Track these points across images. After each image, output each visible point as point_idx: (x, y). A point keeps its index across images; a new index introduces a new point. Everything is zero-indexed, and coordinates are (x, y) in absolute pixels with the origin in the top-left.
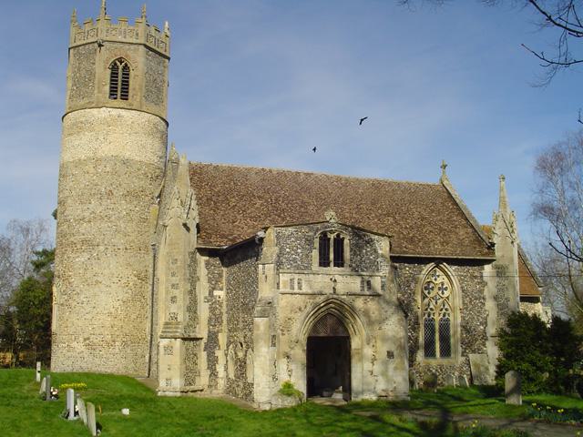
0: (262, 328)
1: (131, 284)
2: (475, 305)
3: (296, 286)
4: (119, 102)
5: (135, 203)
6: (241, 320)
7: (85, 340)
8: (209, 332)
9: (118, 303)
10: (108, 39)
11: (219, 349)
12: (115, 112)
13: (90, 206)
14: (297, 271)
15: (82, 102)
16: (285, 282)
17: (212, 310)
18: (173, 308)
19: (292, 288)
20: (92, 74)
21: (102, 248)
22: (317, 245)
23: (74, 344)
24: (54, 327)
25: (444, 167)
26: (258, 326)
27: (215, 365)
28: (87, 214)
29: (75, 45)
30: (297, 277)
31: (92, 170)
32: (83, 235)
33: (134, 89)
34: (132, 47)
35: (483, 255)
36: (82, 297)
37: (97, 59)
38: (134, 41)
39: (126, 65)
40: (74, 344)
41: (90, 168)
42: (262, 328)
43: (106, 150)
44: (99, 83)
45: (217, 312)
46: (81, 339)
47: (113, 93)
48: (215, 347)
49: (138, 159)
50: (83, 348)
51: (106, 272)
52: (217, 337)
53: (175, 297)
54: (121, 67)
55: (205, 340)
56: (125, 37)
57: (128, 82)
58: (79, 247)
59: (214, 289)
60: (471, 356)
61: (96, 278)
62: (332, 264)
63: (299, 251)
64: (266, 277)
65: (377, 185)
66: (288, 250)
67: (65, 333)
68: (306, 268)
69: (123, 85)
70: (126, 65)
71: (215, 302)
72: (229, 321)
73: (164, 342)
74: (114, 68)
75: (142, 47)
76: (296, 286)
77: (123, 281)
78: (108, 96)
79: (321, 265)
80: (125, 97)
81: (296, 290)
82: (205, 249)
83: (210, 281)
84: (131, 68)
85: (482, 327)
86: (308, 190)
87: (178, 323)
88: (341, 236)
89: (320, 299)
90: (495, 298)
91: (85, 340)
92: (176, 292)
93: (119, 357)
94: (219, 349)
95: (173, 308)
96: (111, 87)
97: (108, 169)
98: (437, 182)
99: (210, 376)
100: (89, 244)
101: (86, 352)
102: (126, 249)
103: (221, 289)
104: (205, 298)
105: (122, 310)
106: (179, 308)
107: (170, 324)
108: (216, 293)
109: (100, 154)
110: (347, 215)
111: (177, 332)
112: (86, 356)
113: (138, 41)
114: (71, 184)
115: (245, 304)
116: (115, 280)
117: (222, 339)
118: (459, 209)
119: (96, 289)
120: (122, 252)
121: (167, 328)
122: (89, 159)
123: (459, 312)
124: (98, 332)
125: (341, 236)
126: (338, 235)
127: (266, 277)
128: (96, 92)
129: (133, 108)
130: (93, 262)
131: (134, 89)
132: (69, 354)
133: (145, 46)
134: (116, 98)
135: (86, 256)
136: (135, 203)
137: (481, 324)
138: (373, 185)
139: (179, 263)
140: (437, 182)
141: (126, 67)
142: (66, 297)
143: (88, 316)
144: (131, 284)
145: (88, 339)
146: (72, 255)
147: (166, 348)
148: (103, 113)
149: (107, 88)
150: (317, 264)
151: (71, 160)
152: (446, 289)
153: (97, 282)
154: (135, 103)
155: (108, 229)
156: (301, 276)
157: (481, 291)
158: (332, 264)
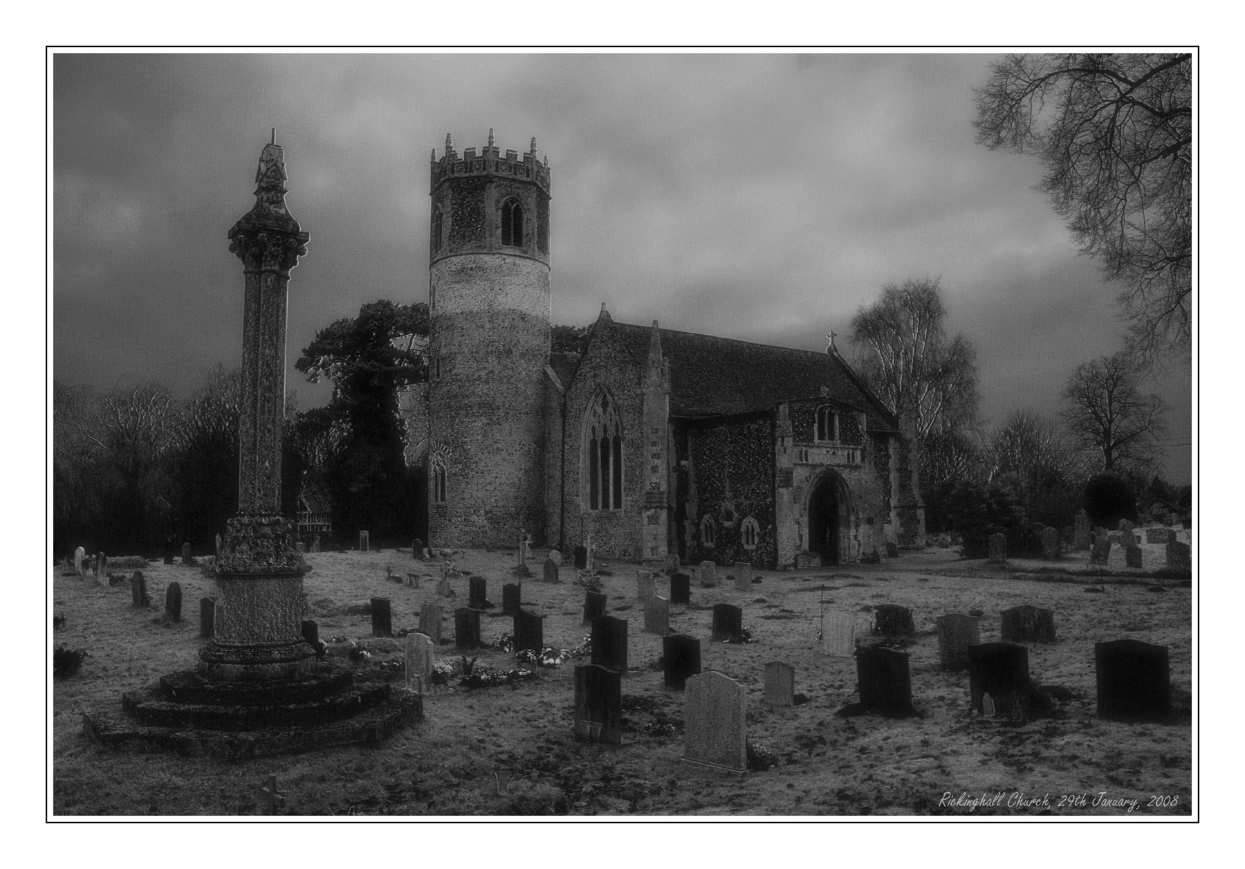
6: (727, 488)
47: (506, 241)
74: (506, 209)
87: (662, 493)
90: (899, 470)
91: (487, 513)
92: (657, 462)
100: (488, 407)
103: (687, 459)
108: (683, 463)
139: (660, 433)
141: (517, 208)
143: (489, 487)
151: (458, 311)
153: (498, 449)
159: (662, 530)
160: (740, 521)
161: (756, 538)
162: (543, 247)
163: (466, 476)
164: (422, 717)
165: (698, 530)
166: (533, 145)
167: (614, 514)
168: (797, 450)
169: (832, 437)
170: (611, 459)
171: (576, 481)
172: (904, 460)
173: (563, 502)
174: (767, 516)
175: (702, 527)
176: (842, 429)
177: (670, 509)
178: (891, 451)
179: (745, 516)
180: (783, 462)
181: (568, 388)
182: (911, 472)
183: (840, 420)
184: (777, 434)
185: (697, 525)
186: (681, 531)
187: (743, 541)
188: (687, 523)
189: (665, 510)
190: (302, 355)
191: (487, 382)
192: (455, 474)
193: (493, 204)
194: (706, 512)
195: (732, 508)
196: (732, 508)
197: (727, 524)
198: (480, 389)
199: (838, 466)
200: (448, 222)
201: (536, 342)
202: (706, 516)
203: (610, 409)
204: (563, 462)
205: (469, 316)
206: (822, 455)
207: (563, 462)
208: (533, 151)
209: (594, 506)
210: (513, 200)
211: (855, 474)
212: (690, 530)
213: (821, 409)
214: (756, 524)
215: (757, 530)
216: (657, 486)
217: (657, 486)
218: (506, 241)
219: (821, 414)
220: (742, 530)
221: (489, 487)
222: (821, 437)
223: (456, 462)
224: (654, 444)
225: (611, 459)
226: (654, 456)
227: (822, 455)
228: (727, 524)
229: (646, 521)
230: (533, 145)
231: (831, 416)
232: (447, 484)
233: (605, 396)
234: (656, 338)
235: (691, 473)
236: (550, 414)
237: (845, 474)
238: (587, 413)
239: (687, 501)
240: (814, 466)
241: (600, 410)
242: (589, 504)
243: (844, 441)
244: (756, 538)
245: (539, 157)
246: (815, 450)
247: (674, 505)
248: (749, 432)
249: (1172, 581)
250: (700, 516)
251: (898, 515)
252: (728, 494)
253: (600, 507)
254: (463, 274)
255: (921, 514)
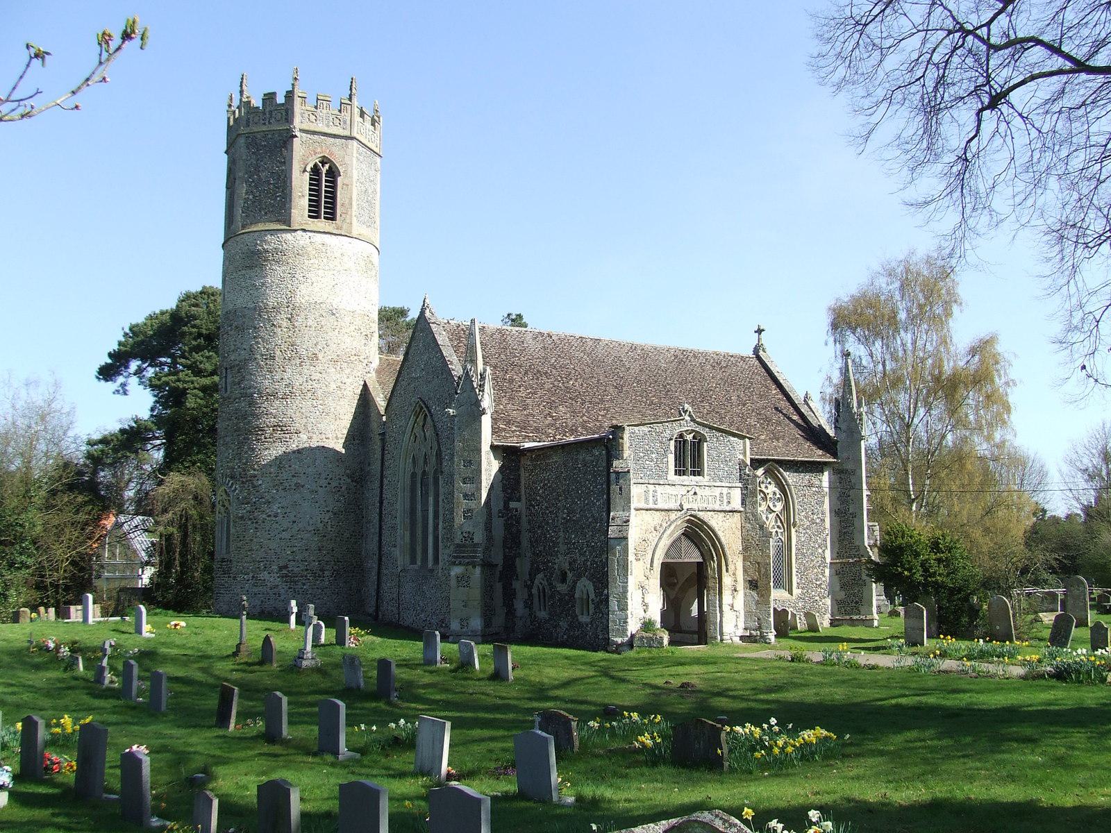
3: (651, 501)
4: (321, 224)
7: (281, 568)
8: (505, 556)
17: (508, 527)
19: (647, 500)
23: (264, 575)
25: (759, 331)
33: (343, 205)
40: (264, 575)
45: (514, 530)
46: (275, 568)
55: (500, 568)
61: (295, 480)
63: (654, 456)
64: (621, 489)
65: (682, 358)
67: (248, 559)
73: (456, 571)
78: (307, 213)
79: (678, 473)
80: (331, 216)
81: (651, 506)
91: (281, 568)
94: (517, 579)
103: (519, 500)
108: (513, 505)
111: (475, 557)
115: (109, 565)
116: (323, 482)
127: (621, 489)
132: (255, 590)
142: (248, 507)
143: (284, 535)
145: (286, 567)
147: (459, 579)
153: (298, 486)
160: (575, 583)
161: (591, 606)
164: (954, 375)
165: (531, 595)
170: (431, 499)
171: (394, 528)
175: (534, 591)
177: (487, 566)
179: (579, 576)
185: (530, 588)
186: (509, 595)
188: (517, 585)
190: (112, 351)
192: (242, 518)
197: (563, 588)
202: (540, 576)
204: (381, 503)
207: (381, 503)
209: (413, 561)
210: (324, 161)
212: (521, 595)
214: (591, 588)
215: (592, 596)
218: (314, 213)
220: (577, 596)
221: (284, 535)
225: (431, 499)
228: (563, 588)
232: (232, 531)
238: (407, 436)
242: (408, 558)
244: (591, 606)
247: (498, 559)
250: (532, 577)
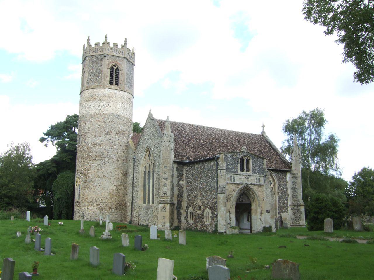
0: (222, 198)
1: (120, 178)
2: (283, 191)
3: (232, 180)
4: (114, 86)
5: (122, 137)
6: (199, 195)
7: (97, 205)
9: (114, 187)
10: (108, 53)
11: (182, 209)
12: (113, 91)
13: (100, 138)
14: (233, 173)
15: (94, 85)
16: (228, 178)
17: (179, 190)
18: (165, 189)
19: (231, 181)
20: (101, 71)
21: (106, 159)
22: (240, 162)
23: (91, 207)
24: (76, 199)
25: (263, 126)
26: (220, 198)
27: (180, 217)
28: (98, 142)
29: (90, 55)
30: (232, 176)
31: (101, 120)
32: (97, 152)
33: (121, 80)
34: (120, 59)
35: (287, 169)
36: (96, 184)
37: (103, 63)
38: (121, 56)
39: (117, 68)
40: (91, 207)
41: (100, 118)
42: (222, 198)
43: (109, 110)
44: (104, 76)
46: (95, 205)
47: (111, 83)
48: (180, 208)
49: (123, 115)
50: (96, 210)
51: (109, 171)
52: (181, 203)
53: (166, 184)
54: (115, 68)
55: (176, 205)
56: (117, 54)
57: (118, 76)
58: (94, 158)
59: (180, 180)
60: (282, 214)
61: (103, 174)
62: (245, 171)
63: (233, 164)
66: (229, 164)
68: (236, 172)
69: (113, 79)
70: (117, 68)
71: (180, 187)
72: (188, 196)
73: (161, 206)
74: (112, 69)
75: (125, 60)
76: (232, 180)
77: (117, 176)
80: (117, 84)
81: (232, 182)
82: (178, 161)
83: (178, 177)
84: (120, 70)
85: (286, 201)
86: (210, 135)
87: (168, 197)
88: (249, 158)
89: (240, 187)
90: (292, 188)
91: (97, 205)
92: (166, 182)
93: (114, 214)
95: (165, 189)
96: (110, 78)
97: (110, 120)
98: (259, 133)
99: (178, 222)
100: (99, 157)
101: (98, 212)
102: (118, 160)
103: (183, 181)
104: (176, 185)
105: (116, 191)
106: (168, 189)
107: (164, 197)
108: (181, 182)
109: (105, 112)
110: (229, 148)
112: (98, 213)
113: (123, 56)
114: (89, 126)
116: (113, 175)
117: (184, 204)
118: (272, 147)
119: (103, 180)
120: (116, 161)
121: (162, 199)
122: (99, 114)
123: (277, 194)
124: (104, 201)
125: (249, 158)
126: (247, 158)
127: (222, 175)
128: (103, 80)
129: (121, 89)
130: (102, 166)
131: (121, 80)
132: (88, 213)
133: (126, 58)
134: (112, 84)
135: (98, 163)
136: (122, 137)
137: (286, 200)
138: (235, 134)
139: (168, 168)
140: (260, 134)
141: (117, 69)
142: (86, 184)
143: (99, 193)
144: (120, 178)
145: (99, 205)
146: (91, 162)
148: (107, 91)
149: (108, 79)
150: (240, 170)
151: (89, 114)
152: (272, 183)
153: (104, 176)
154: (122, 87)
155: (109, 150)
156: (235, 176)
157: (286, 185)
158: (245, 171)
159: (167, 213)
160: (204, 210)
162: (131, 86)
163: (88, 188)
165: (187, 215)
166: (126, 41)
167: (151, 206)
168: (228, 176)
169: (248, 170)
172: (294, 183)
173: (132, 201)
174: (214, 209)
175: (188, 213)
176: (253, 166)
177: (172, 204)
178: (288, 179)
179: (206, 208)
180: (222, 182)
181: (136, 148)
182: (298, 189)
183: (253, 162)
184: (218, 168)
185: (187, 212)
187: (205, 220)
188: (182, 211)
189: (169, 205)
191: (100, 146)
193: (106, 67)
194: (190, 206)
195: (200, 204)
196: (200, 204)
198: (97, 148)
199: (251, 184)
200: (87, 75)
201: (123, 128)
203: (151, 158)
205: (93, 116)
206: (242, 179)
208: (125, 44)
209: (144, 203)
211: (260, 189)
212: (184, 215)
213: (242, 157)
214: (210, 212)
215: (211, 215)
216: (166, 193)
217: (166, 193)
219: (242, 160)
220: (205, 215)
222: (242, 170)
223: (86, 181)
224: (165, 173)
226: (165, 179)
227: (242, 179)
228: (199, 212)
229: (160, 210)
230: (126, 41)
231: (248, 161)
233: (150, 152)
234: (168, 125)
235: (185, 188)
236: (127, 161)
237: (255, 188)
238: (143, 159)
239: (183, 201)
240: (238, 184)
241: (147, 157)
243: (254, 172)
244: (210, 219)
245: (129, 46)
246: (238, 176)
248: (208, 167)
249: (248, 234)
251: (292, 209)
252: (199, 198)
253: (146, 203)
254: (94, 98)
255: (303, 209)
